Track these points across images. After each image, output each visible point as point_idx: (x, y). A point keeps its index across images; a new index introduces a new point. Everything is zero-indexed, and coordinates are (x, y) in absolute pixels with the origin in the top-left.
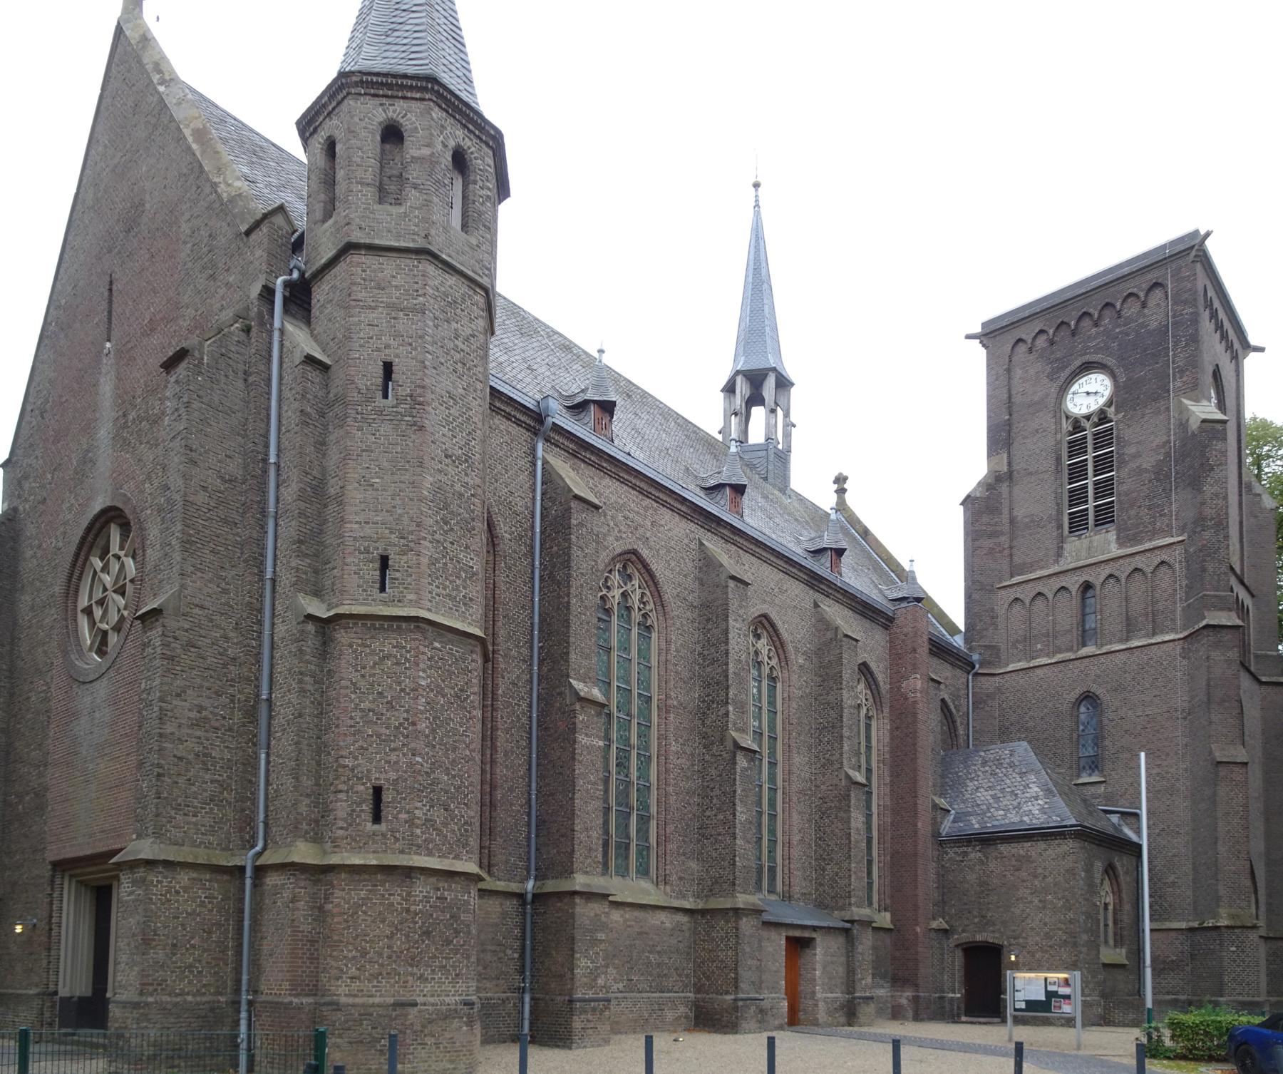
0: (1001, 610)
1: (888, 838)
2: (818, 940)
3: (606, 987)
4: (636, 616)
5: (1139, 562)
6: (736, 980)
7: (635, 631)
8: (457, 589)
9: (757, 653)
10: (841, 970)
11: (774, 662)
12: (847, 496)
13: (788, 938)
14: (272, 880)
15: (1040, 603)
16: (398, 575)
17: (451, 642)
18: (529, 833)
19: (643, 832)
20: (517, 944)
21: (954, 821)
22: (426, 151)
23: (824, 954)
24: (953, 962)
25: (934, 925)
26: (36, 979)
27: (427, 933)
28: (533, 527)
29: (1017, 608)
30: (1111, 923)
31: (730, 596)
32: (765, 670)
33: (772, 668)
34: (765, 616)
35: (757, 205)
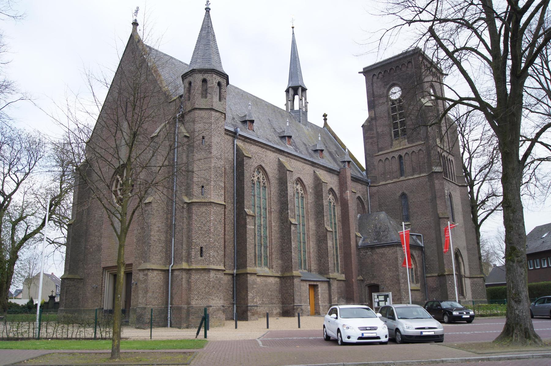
0: (376, 163)
1: (342, 248)
2: (319, 285)
3: (256, 302)
4: (262, 184)
5: (414, 149)
6: (294, 299)
7: (261, 188)
8: (219, 193)
9: (297, 189)
10: (327, 295)
11: (302, 192)
12: (327, 121)
13: (310, 285)
14: (176, 273)
15: (387, 161)
16: (206, 191)
17: (218, 207)
18: (234, 255)
19: (265, 252)
20: (232, 290)
21: (363, 241)
22: (212, 85)
23: (322, 289)
24: (365, 291)
25: (359, 278)
26: (97, 304)
27: (214, 287)
28: (234, 164)
29: (381, 163)
30: (414, 275)
31: (288, 176)
32: (300, 195)
33: (302, 194)
34: (299, 178)
35: (293, 34)
